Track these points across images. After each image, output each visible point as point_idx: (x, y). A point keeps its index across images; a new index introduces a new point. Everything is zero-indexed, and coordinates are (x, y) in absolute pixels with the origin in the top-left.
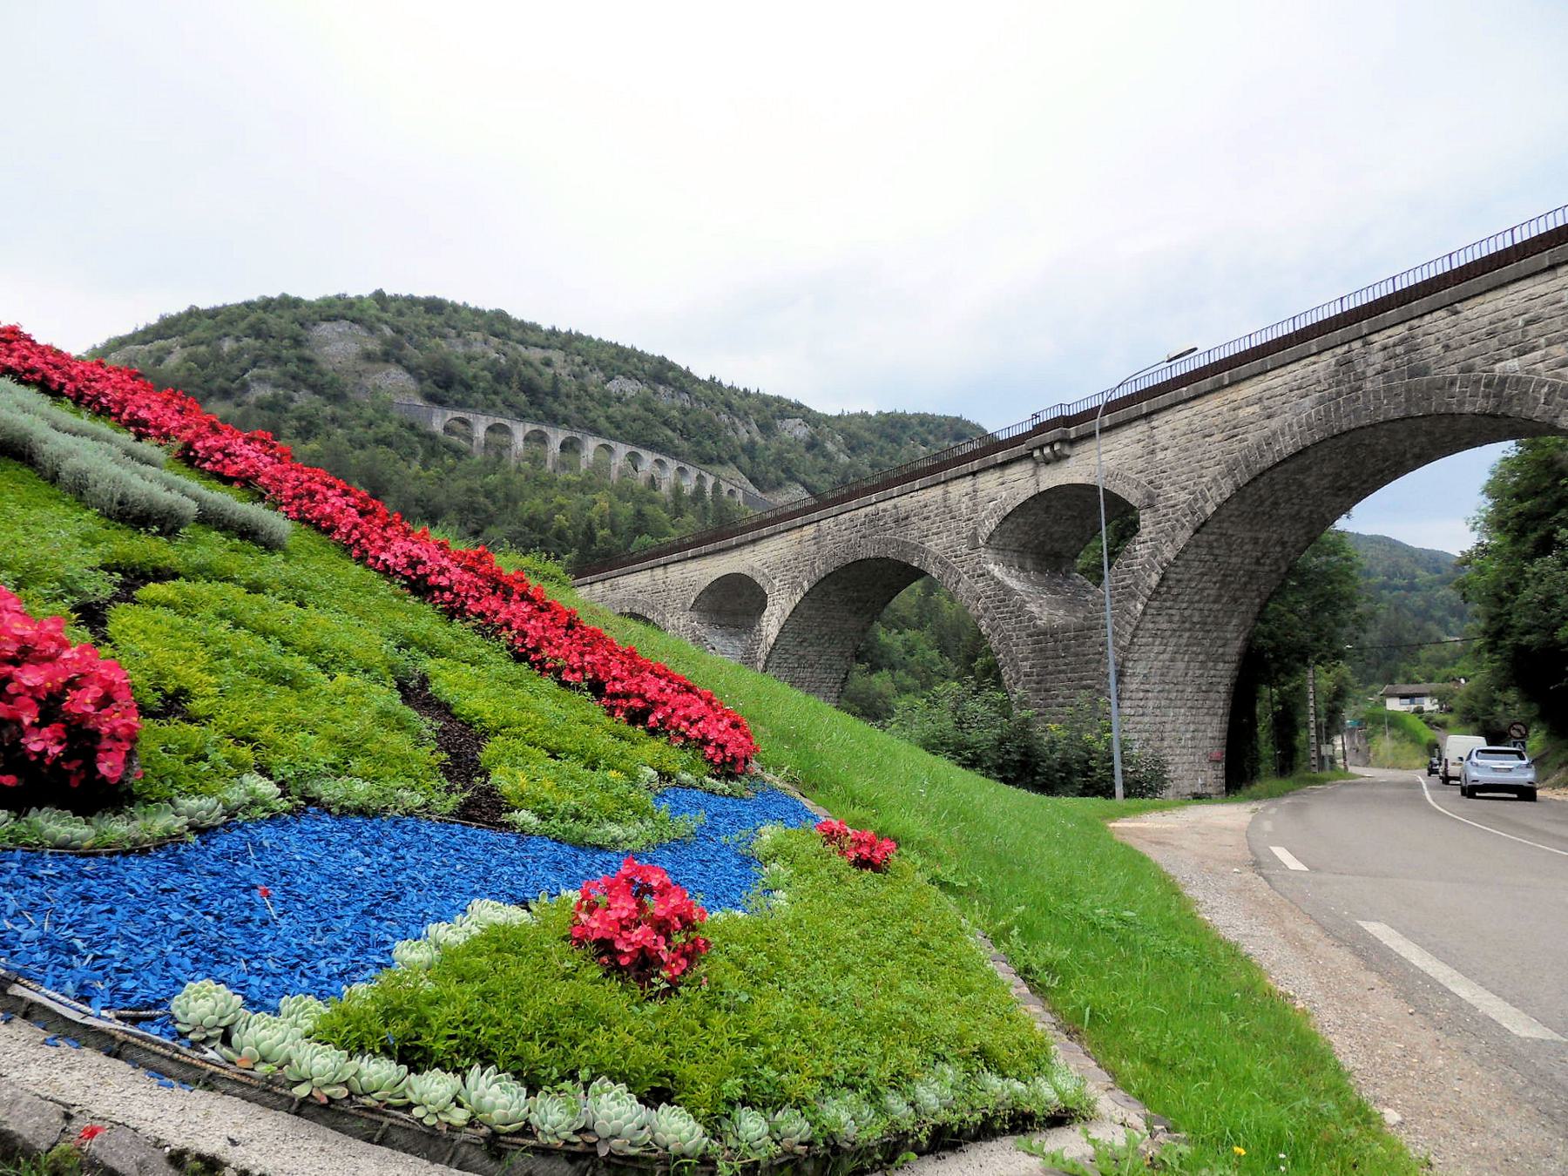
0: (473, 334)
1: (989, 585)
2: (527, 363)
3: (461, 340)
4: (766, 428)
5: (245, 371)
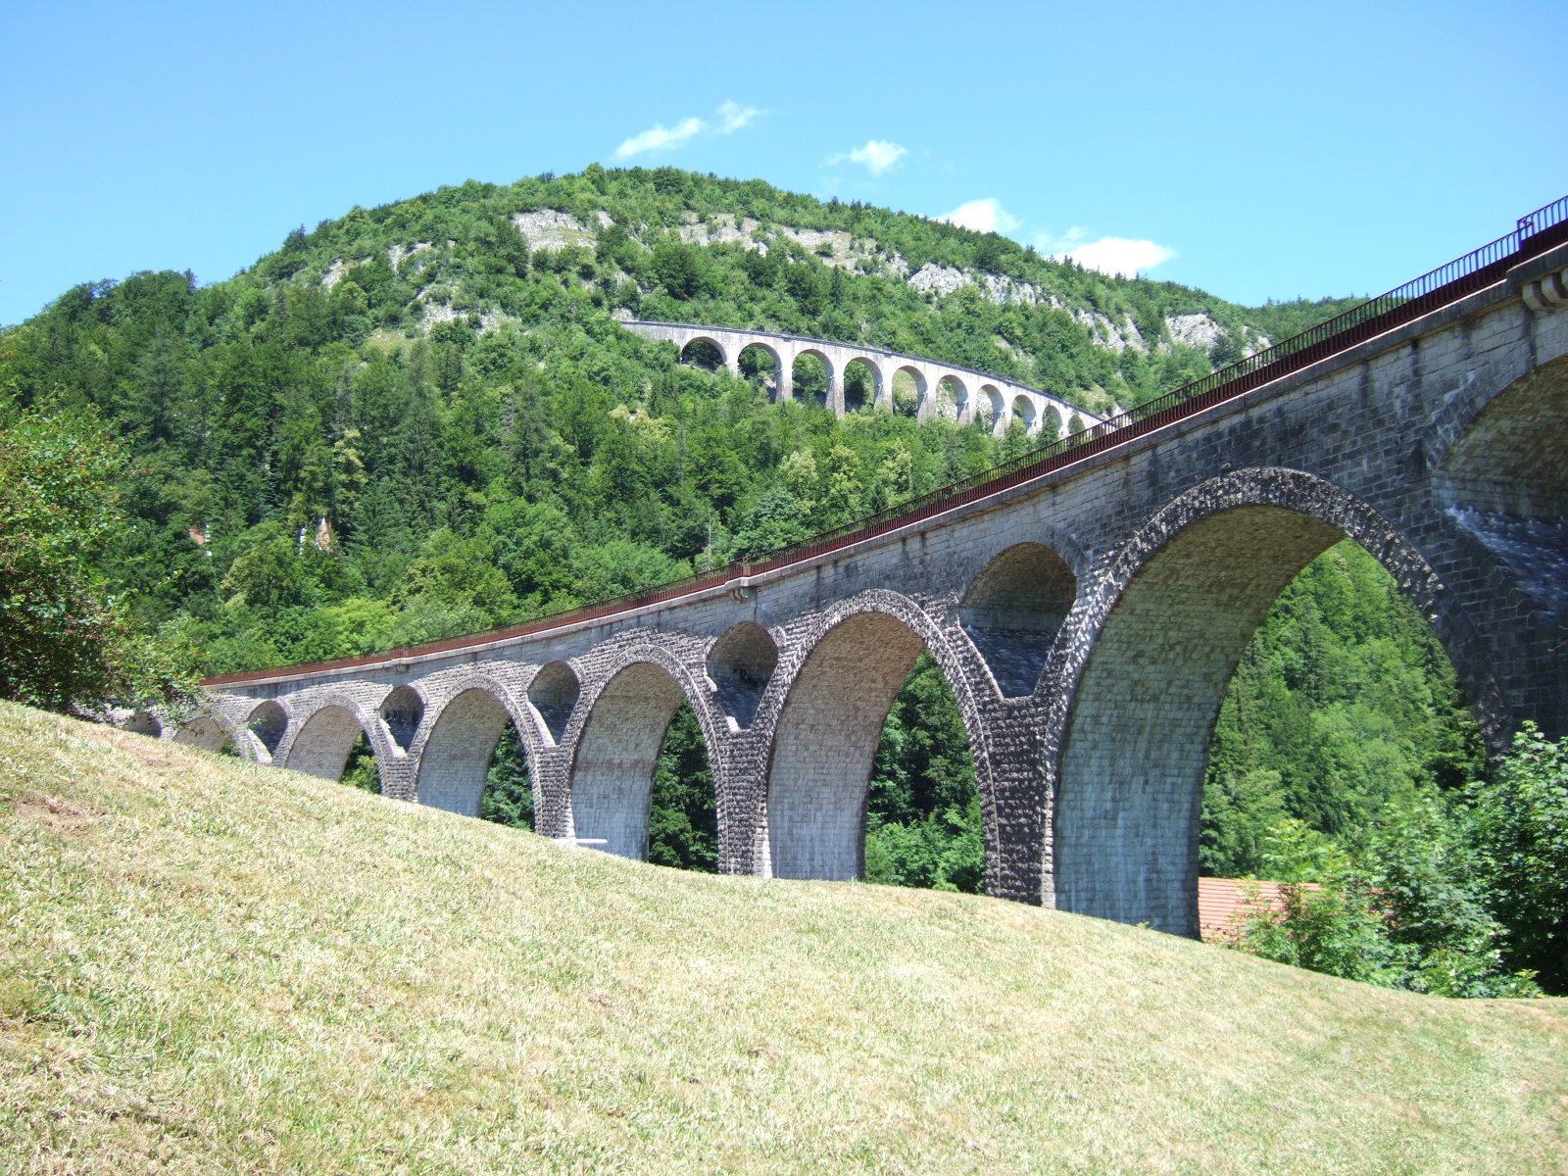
0: (722, 217)
1: (1444, 547)
2: (798, 253)
3: (704, 226)
4: (1151, 330)
5: (420, 289)
